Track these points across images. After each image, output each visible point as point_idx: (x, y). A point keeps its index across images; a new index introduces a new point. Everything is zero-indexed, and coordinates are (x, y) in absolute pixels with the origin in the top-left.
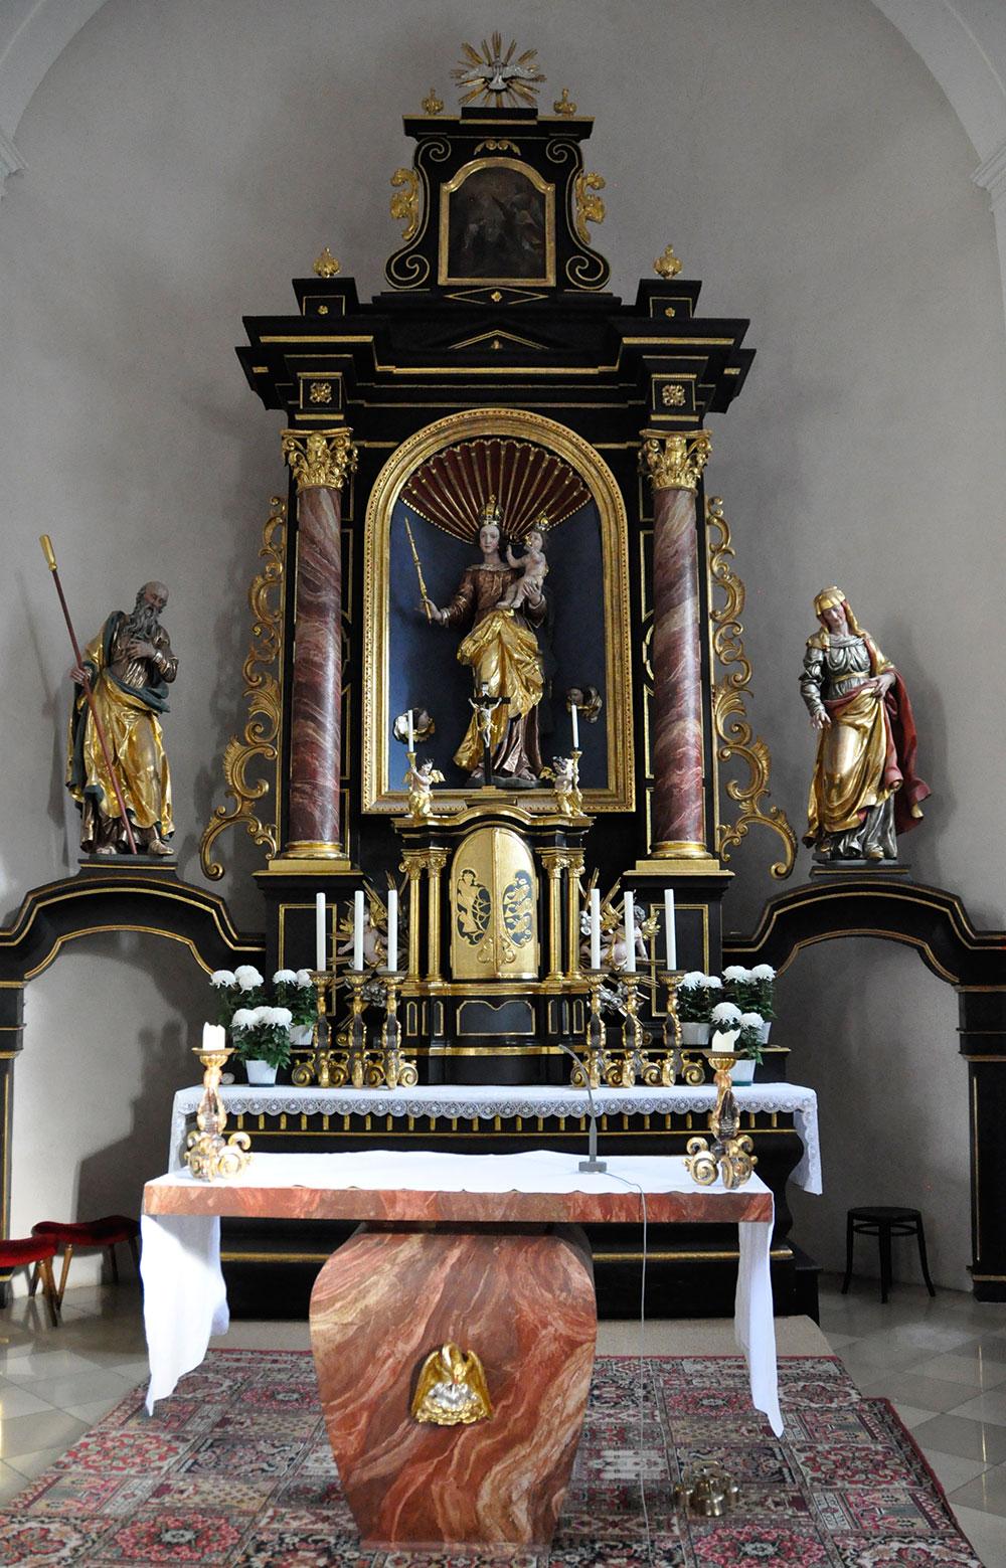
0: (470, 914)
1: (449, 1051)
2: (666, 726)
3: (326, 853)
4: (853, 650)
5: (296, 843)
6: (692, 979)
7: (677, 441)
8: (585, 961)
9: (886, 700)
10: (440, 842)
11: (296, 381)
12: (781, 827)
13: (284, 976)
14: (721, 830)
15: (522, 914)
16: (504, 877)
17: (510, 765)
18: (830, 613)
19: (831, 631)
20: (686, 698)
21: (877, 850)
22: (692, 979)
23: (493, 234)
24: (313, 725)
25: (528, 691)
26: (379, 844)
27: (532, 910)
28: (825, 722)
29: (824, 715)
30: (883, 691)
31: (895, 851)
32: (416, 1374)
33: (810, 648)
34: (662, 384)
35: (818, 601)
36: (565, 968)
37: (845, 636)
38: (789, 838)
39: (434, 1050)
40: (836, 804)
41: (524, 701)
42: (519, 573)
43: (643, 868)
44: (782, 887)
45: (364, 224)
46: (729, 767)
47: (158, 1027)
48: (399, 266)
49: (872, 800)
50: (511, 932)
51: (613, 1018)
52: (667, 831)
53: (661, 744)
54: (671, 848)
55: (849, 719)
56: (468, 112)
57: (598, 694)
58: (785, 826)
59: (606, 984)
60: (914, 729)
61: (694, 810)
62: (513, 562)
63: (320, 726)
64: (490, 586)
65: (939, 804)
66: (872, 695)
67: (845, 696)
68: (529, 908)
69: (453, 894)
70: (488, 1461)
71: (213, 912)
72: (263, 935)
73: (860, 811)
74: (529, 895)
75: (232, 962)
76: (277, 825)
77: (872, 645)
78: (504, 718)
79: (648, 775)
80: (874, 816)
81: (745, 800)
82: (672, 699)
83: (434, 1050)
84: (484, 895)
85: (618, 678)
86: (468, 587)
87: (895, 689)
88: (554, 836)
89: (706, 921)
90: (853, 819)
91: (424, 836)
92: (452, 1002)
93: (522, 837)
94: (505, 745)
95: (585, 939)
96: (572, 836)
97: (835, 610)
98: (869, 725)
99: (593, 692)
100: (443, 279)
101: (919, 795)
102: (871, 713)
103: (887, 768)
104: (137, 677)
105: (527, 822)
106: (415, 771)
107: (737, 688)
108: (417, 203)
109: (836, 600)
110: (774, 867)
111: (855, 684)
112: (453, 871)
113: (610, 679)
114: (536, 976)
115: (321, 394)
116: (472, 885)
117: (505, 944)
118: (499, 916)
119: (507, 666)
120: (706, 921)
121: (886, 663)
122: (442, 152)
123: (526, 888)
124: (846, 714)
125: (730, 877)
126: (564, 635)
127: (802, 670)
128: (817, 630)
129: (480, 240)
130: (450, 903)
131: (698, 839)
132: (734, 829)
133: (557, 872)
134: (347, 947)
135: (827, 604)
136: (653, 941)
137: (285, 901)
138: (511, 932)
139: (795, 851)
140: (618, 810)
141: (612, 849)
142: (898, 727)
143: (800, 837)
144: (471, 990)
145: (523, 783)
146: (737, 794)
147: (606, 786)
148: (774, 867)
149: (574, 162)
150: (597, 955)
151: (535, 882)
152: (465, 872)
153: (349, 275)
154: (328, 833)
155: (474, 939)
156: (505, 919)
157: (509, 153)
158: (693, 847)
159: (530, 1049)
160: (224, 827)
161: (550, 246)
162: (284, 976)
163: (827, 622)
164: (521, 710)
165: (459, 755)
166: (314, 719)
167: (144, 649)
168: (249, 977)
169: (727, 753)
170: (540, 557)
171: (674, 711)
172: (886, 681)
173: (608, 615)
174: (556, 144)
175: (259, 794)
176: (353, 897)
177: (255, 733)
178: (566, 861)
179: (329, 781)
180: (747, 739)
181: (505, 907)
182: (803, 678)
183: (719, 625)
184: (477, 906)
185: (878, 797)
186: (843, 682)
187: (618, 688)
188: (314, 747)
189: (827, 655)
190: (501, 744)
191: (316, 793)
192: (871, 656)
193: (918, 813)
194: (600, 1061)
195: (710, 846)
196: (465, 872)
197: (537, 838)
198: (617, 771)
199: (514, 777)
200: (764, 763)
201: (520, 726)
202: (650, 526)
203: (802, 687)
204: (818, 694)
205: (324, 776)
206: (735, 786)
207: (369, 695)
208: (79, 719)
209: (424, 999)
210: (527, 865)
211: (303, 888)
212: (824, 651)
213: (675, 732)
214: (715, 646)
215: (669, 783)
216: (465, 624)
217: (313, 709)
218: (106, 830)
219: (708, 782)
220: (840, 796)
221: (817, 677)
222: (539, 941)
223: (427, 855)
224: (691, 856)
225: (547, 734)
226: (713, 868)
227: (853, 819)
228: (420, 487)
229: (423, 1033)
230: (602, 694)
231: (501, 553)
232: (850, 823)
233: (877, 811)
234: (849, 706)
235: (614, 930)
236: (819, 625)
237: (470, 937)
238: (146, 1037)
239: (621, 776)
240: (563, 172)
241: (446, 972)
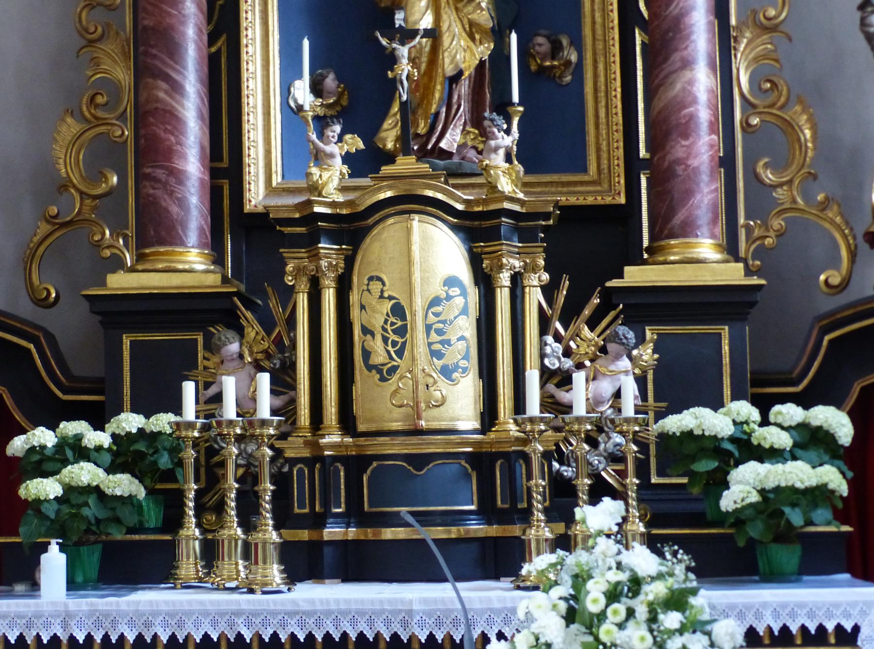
0: (379, 338)
1: (352, 533)
2: (666, 77)
3: (192, 265)
5: (147, 251)
10: (335, 238)
14: (747, 227)
15: (454, 339)
20: (694, 37)
24: (164, 85)
25: (473, 39)
26: (254, 240)
38: (845, 237)
41: (463, 53)
43: (635, 276)
44: (829, 304)
46: (755, 136)
50: (439, 363)
52: (669, 225)
53: (659, 104)
54: (676, 248)
57: (571, 43)
61: (706, 194)
63: (176, 88)
68: (466, 328)
69: (355, 314)
71: (31, 346)
72: (101, 380)
74: (464, 311)
76: (131, 232)
78: (440, 79)
79: (643, 153)
81: (781, 185)
82: (673, 39)
85: (598, 19)
88: (498, 227)
89: (726, 349)
91: (310, 228)
92: (356, 464)
93: (454, 228)
94: (443, 115)
96: (525, 225)
99: (565, 42)
105: (460, 207)
106: (314, 137)
107: (769, 28)
110: (822, 277)
112: (355, 279)
113: (587, 21)
114: (476, 425)
116: (381, 297)
117: (431, 381)
120: (726, 349)
123: (459, 301)
125: (760, 287)
130: (351, 325)
131: (713, 236)
132: (766, 226)
133: (505, 278)
134: (212, 391)
136: (650, 376)
137: (131, 330)
138: (439, 363)
139: (853, 255)
140: (600, 201)
143: (860, 232)
145: (467, 167)
146: (769, 176)
147: (585, 170)
148: (822, 277)
151: (473, 294)
152: (371, 279)
153: (748, 626)
154: (192, 237)
156: (430, 344)
158: (706, 248)
160: (57, 234)
164: (463, 66)
165: (383, 134)
166: (168, 79)
169: (755, 121)
171: (676, 57)
175: (103, 188)
177: (97, 106)
179: (193, 164)
180: (783, 99)
181: (428, 328)
184: (389, 328)
187: (599, 31)
188: (174, 120)
190: (437, 114)
191: (172, 180)
195: (731, 249)
196: (371, 279)
197: (478, 229)
198: (598, 149)
199: (456, 159)
200: (808, 133)
201: (464, 88)
205: (184, 157)
206: (766, 166)
207: (250, 49)
209: (316, 459)
210: (464, 273)
213: (679, 86)
215: (670, 157)
217: (164, 63)
219: (727, 162)
222: (481, 376)
223: (315, 256)
224: (702, 259)
226: (733, 274)
229: (317, 509)
230: (577, 43)
235: (592, 361)
237: (380, 371)
239: (604, 155)
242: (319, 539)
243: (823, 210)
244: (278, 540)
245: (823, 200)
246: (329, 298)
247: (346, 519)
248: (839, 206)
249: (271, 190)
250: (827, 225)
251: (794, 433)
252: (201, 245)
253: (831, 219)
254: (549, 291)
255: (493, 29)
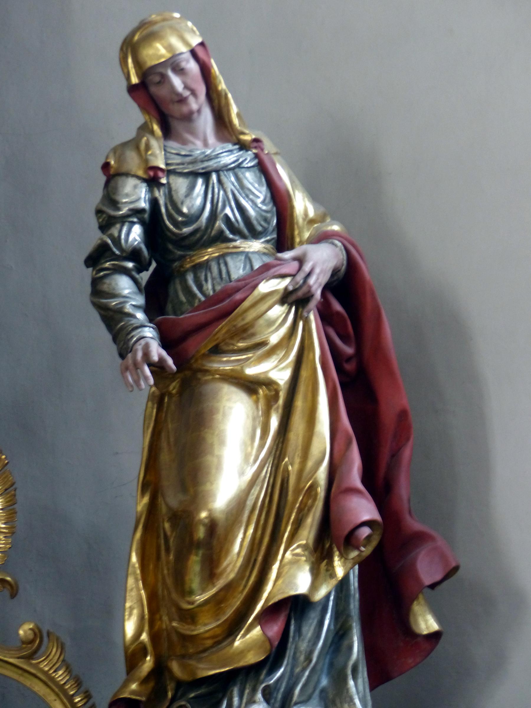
4: (230, 180)
9: (326, 316)
12: (49, 681)
18: (164, 78)
19: (168, 132)
28: (158, 369)
29: (157, 351)
30: (317, 283)
33: (112, 175)
35: (131, 47)
37: (204, 141)
40: (200, 598)
49: (302, 582)
55: (225, 364)
58: (60, 676)
60: (401, 395)
66: (286, 298)
67: (212, 301)
73: (272, 611)
77: (284, 175)
80: (308, 630)
87: (346, 284)
90: (250, 640)
97: (180, 71)
98: (282, 376)
101: (427, 570)
102: (279, 344)
109: (177, 42)
111: (237, 270)
121: (321, 219)
124: (217, 351)
127: (94, 237)
128: (131, 134)
135: (157, 52)
142: (361, 385)
163: (152, 95)
172: (322, 261)
182: (97, 257)
185: (315, 573)
186: (206, 265)
189: (160, 195)
193: (427, 623)
203: (95, 282)
204: (140, 300)
212: (152, 182)
220: (211, 572)
221: (134, 254)
227: (250, 640)
232: (242, 653)
233: (313, 616)
234: (222, 328)
236: (134, 115)
243: (29, 657)
244: (259, 628)
245: (31, 636)
248: (62, 647)
250: (39, 688)
251: (263, 638)
253: (46, 673)
255: (122, 308)
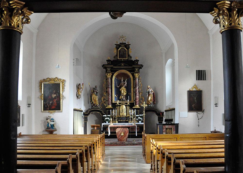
3: (110, 106)
6: (137, 116)
7: (137, 74)
8: (129, 114)
11: (107, 69)
13: (108, 115)
16: (124, 109)
17: (124, 99)
21: (151, 106)
22: (137, 116)
23: (122, 54)
26: (114, 106)
27: (126, 111)
31: (153, 106)
32: (121, 133)
34: (136, 69)
35: (148, 87)
36: (128, 115)
39: (119, 121)
41: (125, 94)
42: (125, 84)
43: (134, 107)
45: (112, 54)
47: (96, 119)
48: (115, 57)
51: (131, 118)
54: (136, 106)
56: (120, 43)
59: (131, 116)
62: (124, 83)
64: (122, 85)
65: (157, 102)
68: (125, 111)
70: (124, 138)
75: (104, 114)
83: (119, 121)
84: (122, 110)
86: (120, 84)
87: (153, 93)
91: (118, 106)
92: (120, 117)
95: (129, 113)
96: (128, 106)
100: (118, 58)
103: (152, 100)
104: (95, 93)
108: (116, 51)
115: (109, 70)
118: (123, 111)
119: (124, 91)
122: (118, 47)
126: (128, 89)
129: (121, 55)
133: (127, 108)
141: (131, 106)
142: (154, 96)
144: (121, 116)
146: (141, 101)
149: (129, 48)
150: (130, 114)
155: (122, 113)
157: (124, 47)
158: (138, 106)
159: (125, 120)
161: (127, 55)
162: (108, 115)
167: (96, 91)
168: (106, 116)
170: (126, 83)
172: (153, 93)
173: (132, 87)
174: (127, 46)
176: (3, 15)
178: (128, 107)
183: (140, 88)
192: (152, 91)
193: (155, 103)
194: (130, 121)
197: (126, 106)
201: (125, 96)
202: (135, 80)
208: (91, 97)
211: (110, 109)
214: (140, 89)
216: (120, 87)
218: (94, 105)
224: (138, 106)
225: (127, 97)
226: (139, 107)
228: (117, 76)
230: (131, 93)
231: (123, 82)
238: (95, 120)
240: (128, 48)
241: (120, 115)
242: (174, 123)
246: (119, 109)
247: (119, 120)
249: (114, 102)
252: (111, 105)
254: (129, 108)
